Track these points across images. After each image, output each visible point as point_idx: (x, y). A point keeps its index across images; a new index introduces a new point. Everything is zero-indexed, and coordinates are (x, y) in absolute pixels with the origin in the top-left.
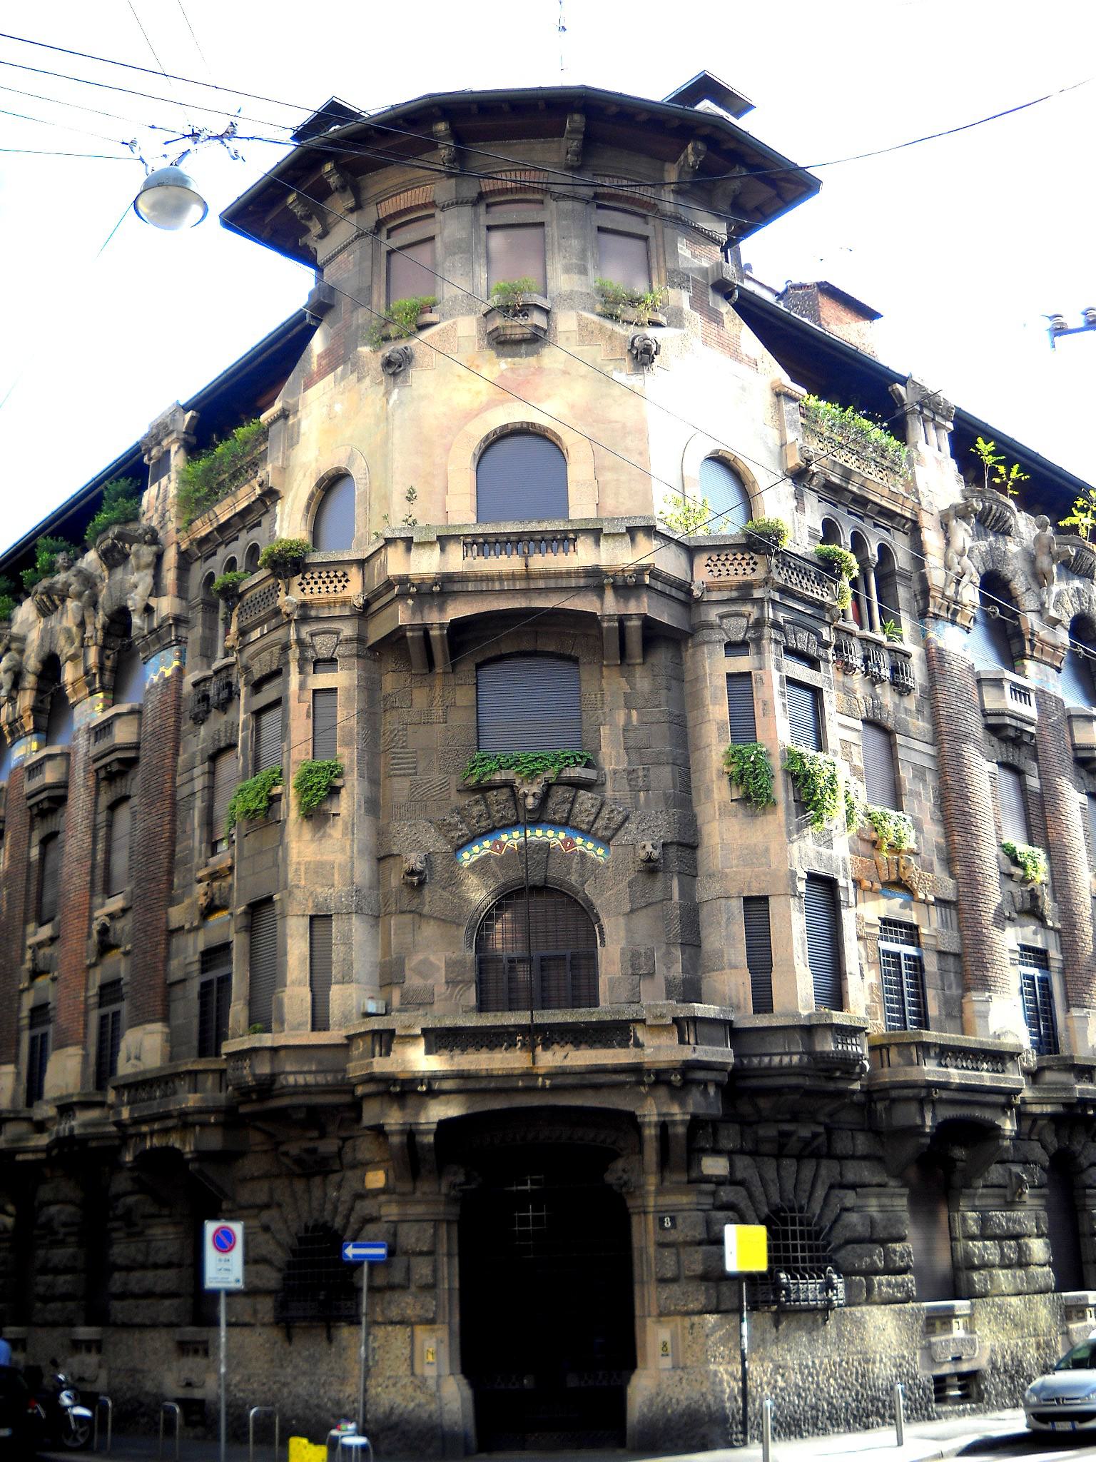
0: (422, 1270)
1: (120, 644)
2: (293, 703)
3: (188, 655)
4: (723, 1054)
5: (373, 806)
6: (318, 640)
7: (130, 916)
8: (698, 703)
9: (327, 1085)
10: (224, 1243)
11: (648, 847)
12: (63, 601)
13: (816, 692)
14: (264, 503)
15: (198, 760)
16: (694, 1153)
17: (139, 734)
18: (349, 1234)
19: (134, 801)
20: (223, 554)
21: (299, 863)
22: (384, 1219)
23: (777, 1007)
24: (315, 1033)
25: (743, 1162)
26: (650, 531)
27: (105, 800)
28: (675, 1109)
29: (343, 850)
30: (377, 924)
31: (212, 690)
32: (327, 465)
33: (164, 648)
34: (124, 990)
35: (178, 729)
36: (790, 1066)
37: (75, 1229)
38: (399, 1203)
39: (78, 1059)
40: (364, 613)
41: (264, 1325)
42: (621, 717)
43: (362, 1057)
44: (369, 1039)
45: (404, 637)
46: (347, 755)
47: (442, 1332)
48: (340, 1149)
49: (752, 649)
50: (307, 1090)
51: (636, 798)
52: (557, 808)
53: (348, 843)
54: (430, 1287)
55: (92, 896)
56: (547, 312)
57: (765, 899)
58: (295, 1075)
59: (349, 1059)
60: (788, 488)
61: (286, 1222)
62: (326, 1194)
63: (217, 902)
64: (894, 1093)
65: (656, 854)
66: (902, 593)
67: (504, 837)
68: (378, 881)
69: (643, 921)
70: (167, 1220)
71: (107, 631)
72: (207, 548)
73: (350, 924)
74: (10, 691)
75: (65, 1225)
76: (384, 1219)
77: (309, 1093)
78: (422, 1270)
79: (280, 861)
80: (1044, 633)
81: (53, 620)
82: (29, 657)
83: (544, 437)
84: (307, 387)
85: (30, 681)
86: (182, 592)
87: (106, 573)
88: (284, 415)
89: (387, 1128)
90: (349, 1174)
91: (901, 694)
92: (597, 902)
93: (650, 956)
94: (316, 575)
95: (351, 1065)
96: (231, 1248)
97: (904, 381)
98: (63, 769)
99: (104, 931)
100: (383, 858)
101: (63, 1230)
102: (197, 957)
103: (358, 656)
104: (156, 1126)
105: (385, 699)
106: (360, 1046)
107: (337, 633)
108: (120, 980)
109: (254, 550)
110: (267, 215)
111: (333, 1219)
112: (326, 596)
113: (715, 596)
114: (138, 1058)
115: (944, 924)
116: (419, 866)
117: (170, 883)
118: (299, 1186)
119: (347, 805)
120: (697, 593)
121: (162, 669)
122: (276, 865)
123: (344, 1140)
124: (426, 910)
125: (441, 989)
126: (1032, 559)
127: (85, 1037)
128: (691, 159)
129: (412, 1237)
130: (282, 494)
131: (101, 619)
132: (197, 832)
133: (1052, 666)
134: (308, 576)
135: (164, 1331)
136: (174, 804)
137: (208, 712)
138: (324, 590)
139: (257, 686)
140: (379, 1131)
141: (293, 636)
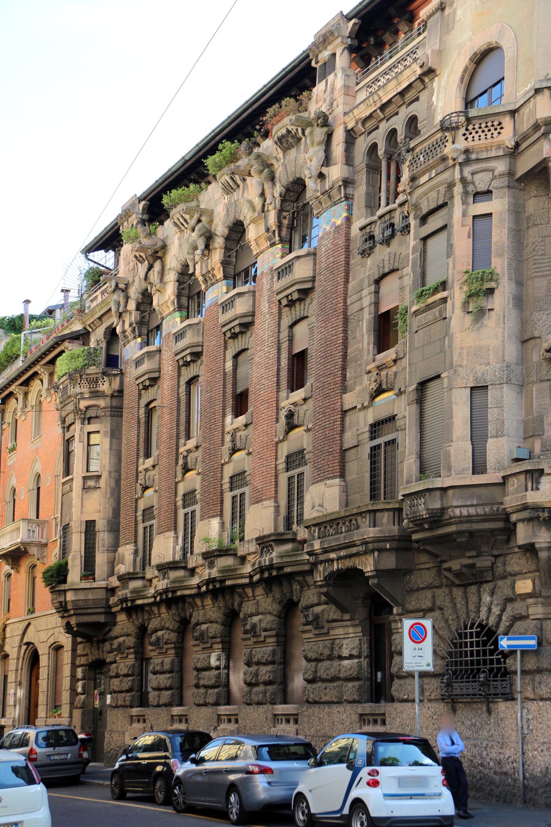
1: (295, 210)
3: (355, 208)
5: (519, 302)
6: (477, 177)
7: (310, 402)
9: (485, 515)
10: (417, 637)
14: (422, 81)
15: (366, 282)
17: (315, 270)
18: (502, 629)
19: (312, 319)
20: (384, 127)
21: (462, 348)
22: (532, 617)
24: (476, 476)
27: (286, 322)
30: (521, 392)
31: (377, 231)
33: (335, 204)
34: (307, 457)
35: (347, 263)
37: (274, 633)
38: (543, 604)
39: (272, 510)
40: (515, 152)
41: (430, 701)
44: (522, 477)
46: (500, 264)
48: (493, 564)
50: (469, 519)
53: (501, 330)
55: (278, 392)
58: (459, 508)
59: (504, 494)
61: (447, 621)
62: (480, 599)
63: (384, 386)
68: (523, 359)
70: (348, 623)
71: (284, 199)
72: (370, 124)
73: (502, 392)
74: (203, 251)
75: (265, 630)
76: (532, 617)
77: (471, 522)
79: (447, 347)
81: (236, 195)
82: (217, 226)
85: (219, 242)
86: (349, 160)
87: (281, 155)
89: (537, 546)
90: (500, 583)
94: (477, 126)
95: (507, 499)
96: (423, 640)
98: (251, 302)
99: (290, 415)
101: (263, 634)
102: (367, 428)
103: (509, 187)
104: (343, 553)
105: (528, 218)
106: (514, 484)
107: (493, 171)
108: (303, 450)
109: (413, 121)
111: (488, 619)
112: (490, 140)
114: (321, 506)
117: (344, 376)
118: (458, 593)
119: (501, 301)
121: (333, 220)
122: (442, 351)
127: (276, 492)
130: (438, 72)
131: (279, 189)
132: (366, 337)
134: (470, 127)
135: (348, 707)
137: (374, 246)
138: (483, 137)
139: (424, 220)
140: (530, 549)
141: (457, 176)
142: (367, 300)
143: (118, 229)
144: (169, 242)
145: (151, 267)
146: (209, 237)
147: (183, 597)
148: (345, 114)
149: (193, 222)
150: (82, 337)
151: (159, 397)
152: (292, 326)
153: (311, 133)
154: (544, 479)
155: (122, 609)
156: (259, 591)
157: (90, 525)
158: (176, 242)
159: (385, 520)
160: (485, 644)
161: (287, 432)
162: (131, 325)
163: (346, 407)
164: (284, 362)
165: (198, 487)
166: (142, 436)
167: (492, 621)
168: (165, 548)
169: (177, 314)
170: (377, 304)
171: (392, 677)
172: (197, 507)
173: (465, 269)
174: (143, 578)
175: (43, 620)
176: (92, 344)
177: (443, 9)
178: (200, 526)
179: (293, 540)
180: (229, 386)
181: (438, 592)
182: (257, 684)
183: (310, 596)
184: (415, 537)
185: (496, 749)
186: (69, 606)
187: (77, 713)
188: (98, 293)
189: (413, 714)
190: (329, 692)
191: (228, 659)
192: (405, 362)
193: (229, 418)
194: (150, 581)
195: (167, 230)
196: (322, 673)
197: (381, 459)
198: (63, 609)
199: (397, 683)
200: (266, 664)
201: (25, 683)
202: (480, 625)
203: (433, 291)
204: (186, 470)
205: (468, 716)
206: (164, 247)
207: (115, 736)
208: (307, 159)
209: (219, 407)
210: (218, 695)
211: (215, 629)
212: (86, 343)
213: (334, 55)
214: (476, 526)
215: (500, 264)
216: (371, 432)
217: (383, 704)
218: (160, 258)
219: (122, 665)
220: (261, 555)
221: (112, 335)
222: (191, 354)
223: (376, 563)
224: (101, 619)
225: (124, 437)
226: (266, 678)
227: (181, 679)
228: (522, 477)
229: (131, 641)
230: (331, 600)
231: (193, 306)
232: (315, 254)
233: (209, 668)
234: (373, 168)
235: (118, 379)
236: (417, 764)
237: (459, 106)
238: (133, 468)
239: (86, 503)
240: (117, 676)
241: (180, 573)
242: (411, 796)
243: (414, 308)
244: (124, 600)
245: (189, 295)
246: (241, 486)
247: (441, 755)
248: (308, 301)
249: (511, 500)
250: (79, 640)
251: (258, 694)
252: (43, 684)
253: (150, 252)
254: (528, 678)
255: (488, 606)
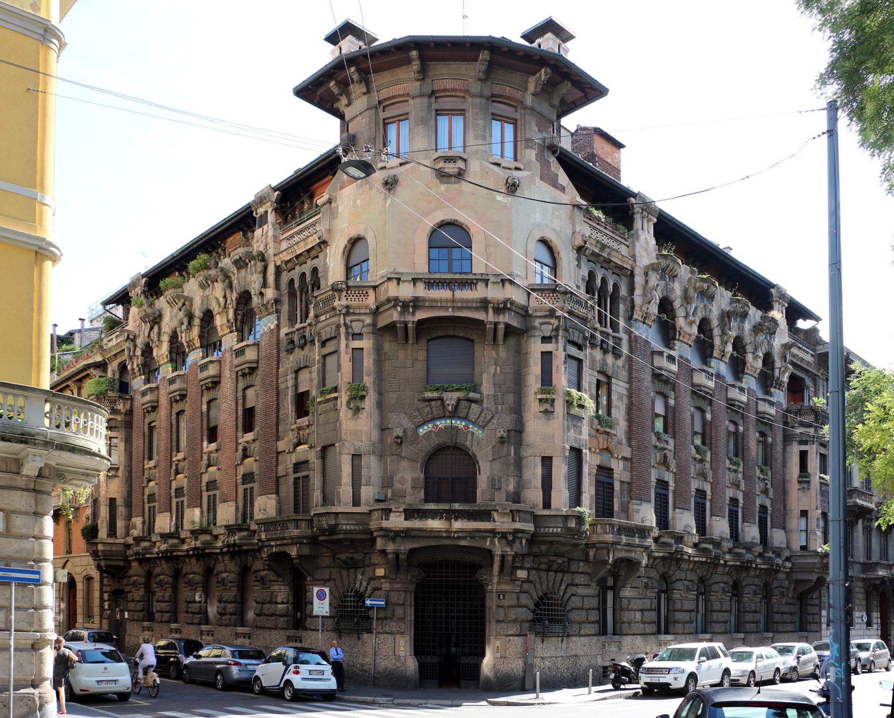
0: (399, 611)
1: (245, 314)
2: (343, 354)
4: (530, 527)
5: (380, 405)
6: (354, 324)
7: (257, 443)
8: (527, 365)
10: (321, 596)
11: (501, 432)
12: (213, 283)
13: (580, 361)
16: (514, 569)
18: (367, 594)
19: (258, 388)
20: (298, 270)
23: (553, 507)
25: (533, 572)
26: (511, 282)
27: (241, 386)
28: (508, 549)
29: (366, 425)
32: (354, 233)
33: (270, 314)
36: (557, 533)
39: (234, 508)
40: (376, 313)
42: (492, 369)
43: (377, 519)
44: (380, 512)
45: (395, 326)
46: (368, 381)
47: (407, 638)
49: (554, 340)
50: (350, 532)
51: (497, 408)
52: (462, 412)
54: (402, 619)
56: (465, 160)
57: (551, 458)
58: (346, 525)
59: (370, 520)
60: (573, 255)
64: (598, 545)
65: (505, 435)
66: (622, 307)
67: (438, 423)
68: (382, 440)
69: (497, 465)
71: (238, 303)
78: (399, 611)
80: (687, 329)
81: (208, 292)
83: (462, 227)
84: (341, 188)
85: (197, 322)
86: (277, 287)
87: (236, 271)
88: (330, 202)
90: (367, 569)
91: (616, 358)
92: (478, 456)
93: (500, 481)
95: (371, 523)
97: (635, 195)
99: (245, 449)
100: (384, 429)
104: (278, 543)
106: (376, 515)
107: (363, 321)
110: (318, 91)
113: (538, 314)
114: (265, 510)
115: (625, 469)
116: (401, 435)
117: (277, 429)
118: (344, 572)
120: (530, 312)
122: (335, 429)
123: (366, 554)
124: (403, 454)
125: (409, 490)
126: (686, 291)
128: (543, 77)
129: (395, 598)
131: (235, 295)
133: (688, 344)
135: (281, 631)
136: (278, 394)
139: (323, 344)
140: (383, 552)
141: (342, 321)
142: (290, 383)
143: (128, 293)
144: (163, 313)
145: (152, 328)
146: (190, 317)
147: (177, 556)
148: (275, 255)
149: (180, 304)
150: (102, 366)
151: (158, 419)
152: (244, 390)
153: (255, 264)
154: (392, 514)
155: (136, 559)
156: (227, 558)
157: (112, 501)
158: (168, 314)
159: (303, 526)
160: (358, 602)
161: (243, 460)
162: (138, 366)
163: (279, 450)
164: (240, 413)
165: (185, 485)
166: (147, 444)
167: (362, 589)
168: (164, 523)
169: (170, 365)
170: (296, 386)
171: (306, 616)
172: (185, 499)
173: (347, 381)
174: (150, 541)
175: (79, 559)
176: (110, 375)
177: (330, 203)
178: (187, 512)
179: (248, 530)
180: (205, 422)
181: (333, 570)
182: (225, 614)
183: (258, 565)
184: (320, 538)
185: (361, 658)
186: (100, 554)
187: (105, 622)
188: (113, 336)
189: (318, 638)
190: (270, 622)
191: (206, 598)
192: (314, 428)
193: (205, 443)
194: (155, 543)
195: (161, 303)
196: (265, 611)
197: (301, 487)
198: (95, 555)
199: (309, 620)
200: (230, 603)
201: (65, 599)
202: (356, 592)
203: (329, 390)
204: (177, 473)
205: (347, 640)
206: (160, 316)
207: (133, 638)
208: (252, 279)
209: (199, 431)
210: (201, 618)
211: (198, 578)
212: (105, 370)
213: (266, 212)
214: (354, 536)
215: (368, 381)
216: (294, 468)
217: (300, 631)
218: (158, 323)
219: (136, 595)
220: (228, 537)
221: (123, 367)
222: (180, 395)
223: (298, 550)
224: (122, 564)
225: (134, 444)
226: (231, 611)
227: (176, 607)
228: (380, 512)
229: (142, 580)
230: (270, 568)
231: (180, 360)
232: (258, 345)
233: (194, 602)
234: (292, 294)
235: (129, 402)
236: (319, 664)
237: (343, 279)
238: (141, 465)
239: (109, 486)
240: (133, 601)
241: (176, 541)
242: (315, 680)
243: (319, 400)
244: (137, 554)
245: (178, 354)
246: (214, 490)
247: (331, 660)
248: (254, 375)
249: (373, 525)
250: (105, 575)
251: (226, 620)
252: (80, 601)
253: (151, 318)
254: (380, 622)
255: (360, 581)
